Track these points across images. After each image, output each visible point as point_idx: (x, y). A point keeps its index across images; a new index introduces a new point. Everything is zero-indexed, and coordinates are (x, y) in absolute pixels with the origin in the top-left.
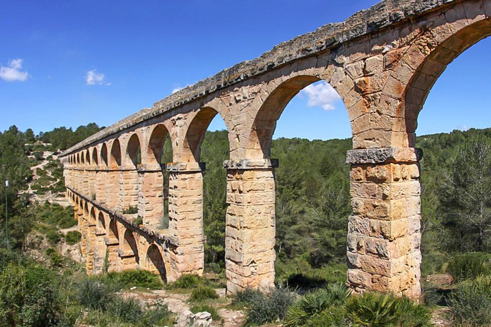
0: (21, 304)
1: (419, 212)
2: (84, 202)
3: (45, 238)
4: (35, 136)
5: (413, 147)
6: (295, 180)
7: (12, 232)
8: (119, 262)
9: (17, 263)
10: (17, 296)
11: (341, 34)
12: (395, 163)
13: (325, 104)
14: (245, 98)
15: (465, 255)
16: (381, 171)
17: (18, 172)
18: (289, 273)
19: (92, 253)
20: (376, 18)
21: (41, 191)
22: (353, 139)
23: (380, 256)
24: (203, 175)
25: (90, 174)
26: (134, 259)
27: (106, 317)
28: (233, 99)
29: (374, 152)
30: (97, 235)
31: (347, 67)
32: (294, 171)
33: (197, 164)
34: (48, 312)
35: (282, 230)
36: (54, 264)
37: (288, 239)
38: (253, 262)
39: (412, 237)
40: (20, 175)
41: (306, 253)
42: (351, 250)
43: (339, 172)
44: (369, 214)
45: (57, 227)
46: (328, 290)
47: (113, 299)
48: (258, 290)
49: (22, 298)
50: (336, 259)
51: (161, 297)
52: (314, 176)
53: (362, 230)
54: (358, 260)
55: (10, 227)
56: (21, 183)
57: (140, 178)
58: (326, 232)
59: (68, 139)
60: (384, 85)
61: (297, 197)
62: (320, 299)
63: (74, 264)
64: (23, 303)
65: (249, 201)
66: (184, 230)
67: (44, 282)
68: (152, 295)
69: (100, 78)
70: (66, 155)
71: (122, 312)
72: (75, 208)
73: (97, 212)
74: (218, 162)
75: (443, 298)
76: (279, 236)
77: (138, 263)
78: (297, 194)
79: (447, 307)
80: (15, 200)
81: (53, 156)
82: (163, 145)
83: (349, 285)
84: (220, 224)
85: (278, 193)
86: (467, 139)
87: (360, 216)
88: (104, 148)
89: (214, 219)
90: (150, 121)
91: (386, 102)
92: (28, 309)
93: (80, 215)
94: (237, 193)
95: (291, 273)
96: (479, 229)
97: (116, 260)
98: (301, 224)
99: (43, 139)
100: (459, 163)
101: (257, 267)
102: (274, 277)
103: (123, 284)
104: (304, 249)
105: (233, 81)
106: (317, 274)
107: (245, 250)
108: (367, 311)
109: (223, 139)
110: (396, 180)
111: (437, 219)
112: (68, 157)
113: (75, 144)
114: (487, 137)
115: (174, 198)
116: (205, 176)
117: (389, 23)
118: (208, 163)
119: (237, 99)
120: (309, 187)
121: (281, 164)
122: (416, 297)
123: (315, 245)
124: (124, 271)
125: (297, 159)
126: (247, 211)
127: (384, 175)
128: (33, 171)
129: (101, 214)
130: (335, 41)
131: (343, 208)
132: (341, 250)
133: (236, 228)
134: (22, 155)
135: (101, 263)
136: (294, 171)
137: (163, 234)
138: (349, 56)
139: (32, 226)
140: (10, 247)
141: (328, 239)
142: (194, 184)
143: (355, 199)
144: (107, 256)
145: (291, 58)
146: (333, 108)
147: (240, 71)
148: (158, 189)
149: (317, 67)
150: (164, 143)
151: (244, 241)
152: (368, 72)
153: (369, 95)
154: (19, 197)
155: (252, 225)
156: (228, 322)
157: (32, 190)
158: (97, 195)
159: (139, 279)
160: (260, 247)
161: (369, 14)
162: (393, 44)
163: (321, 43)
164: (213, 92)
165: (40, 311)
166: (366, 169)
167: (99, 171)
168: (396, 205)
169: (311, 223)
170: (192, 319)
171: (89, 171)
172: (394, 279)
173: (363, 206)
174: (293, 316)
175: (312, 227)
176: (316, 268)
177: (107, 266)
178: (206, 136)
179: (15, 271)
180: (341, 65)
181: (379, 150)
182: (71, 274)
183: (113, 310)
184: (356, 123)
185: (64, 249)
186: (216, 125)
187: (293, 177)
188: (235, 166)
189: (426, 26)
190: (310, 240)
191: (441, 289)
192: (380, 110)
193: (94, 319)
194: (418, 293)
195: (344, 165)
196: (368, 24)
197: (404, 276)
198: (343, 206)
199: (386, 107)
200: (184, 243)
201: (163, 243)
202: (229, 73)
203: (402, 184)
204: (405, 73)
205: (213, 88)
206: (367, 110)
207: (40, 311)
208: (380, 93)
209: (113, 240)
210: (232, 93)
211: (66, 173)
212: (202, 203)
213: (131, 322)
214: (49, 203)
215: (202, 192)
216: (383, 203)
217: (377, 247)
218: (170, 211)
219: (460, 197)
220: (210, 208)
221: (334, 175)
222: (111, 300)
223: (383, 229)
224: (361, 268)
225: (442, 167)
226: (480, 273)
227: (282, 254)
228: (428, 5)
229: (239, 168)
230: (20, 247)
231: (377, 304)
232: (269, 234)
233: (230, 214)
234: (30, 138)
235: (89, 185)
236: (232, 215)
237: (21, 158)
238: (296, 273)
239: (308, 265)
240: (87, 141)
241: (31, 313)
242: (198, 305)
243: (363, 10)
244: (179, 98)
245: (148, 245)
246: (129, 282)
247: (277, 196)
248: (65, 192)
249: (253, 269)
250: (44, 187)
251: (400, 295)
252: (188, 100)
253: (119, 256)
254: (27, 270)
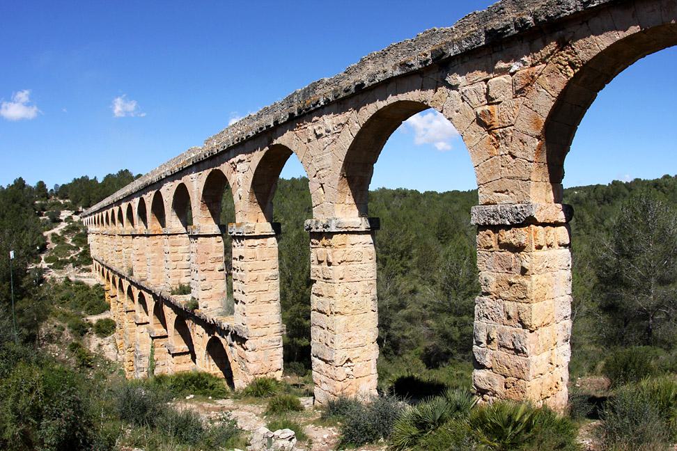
0: (39, 419)
1: (570, 292)
2: (117, 279)
3: (67, 329)
4: (49, 191)
5: (561, 203)
6: (403, 247)
7: (21, 320)
8: (169, 362)
9: (30, 362)
10: (33, 407)
11: (451, 44)
12: (537, 225)
13: (438, 141)
14: (328, 131)
15: (627, 350)
16: (518, 236)
17: (27, 239)
18: (396, 375)
19: (131, 349)
20: (496, 24)
21: (60, 265)
22: (479, 191)
23: (517, 351)
24: (278, 240)
25: (124, 240)
26: (189, 357)
27: (156, 436)
28: (311, 133)
29: (508, 209)
30: (138, 324)
31: (463, 91)
32: (400, 235)
33: (269, 225)
34: (77, 429)
35: (387, 316)
36: (81, 363)
37: (395, 329)
38: (348, 360)
39: (560, 326)
40: (30, 244)
41: (419, 348)
42: (479, 343)
43: (462, 236)
44: (502, 295)
45: (83, 313)
46: (447, 399)
47: (164, 412)
48: (356, 399)
49: (40, 410)
50: (459, 356)
51: (228, 409)
52: (428, 242)
53: (493, 316)
54: (488, 358)
55: (18, 314)
56: (31, 255)
57: (192, 245)
58: (446, 318)
59: (92, 192)
60: (516, 117)
61: (406, 271)
62: (437, 411)
63: (108, 364)
64: (42, 417)
65: (341, 277)
66: (255, 317)
67: (68, 389)
68: (215, 406)
69: (131, 107)
70: (91, 215)
71: (177, 429)
72: (106, 288)
73: (136, 292)
74: (297, 223)
75: (595, 408)
76: (383, 324)
77: (195, 362)
78: (406, 267)
79: (598, 421)
80: (23, 277)
81: (74, 217)
82: (221, 199)
83: (475, 392)
84: (304, 308)
85: (381, 266)
86: (631, 193)
87: (491, 296)
88: (142, 203)
89: (295, 301)
90: (201, 165)
91: (521, 141)
92: (49, 425)
93: (112, 297)
94: (325, 265)
95: (399, 375)
96: (648, 315)
97: (165, 359)
98: (412, 308)
99: (59, 195)
100: (621, 226)
101: (353, 368)
102: (377, 381)
103: (175, 392)
104: (417, 342)
105: (310, 108)
106: (433, 376)
107: (338, 344)
108: (496, 427)
109: (301, 190)
110: (539, 248)
111: (593, 301)
112: (93, 216)
113: (102, 199)
114: (658, 190)
115: (240, 272)
116: (280, 242)
117: (515, 32)
118: (284, 224)
119: (318, 132)
120: (422, 257)
121: (383, 226)
122: (560, 408)
123: (431, 337)
124: (176, 374)
125: (404, 219)
126: (339, 290)
127: (523, 242)
128: (46, 237)
129: (141, 295)
130: (444, 54)
131: (468, 286)
132: (465, 344)
133: (325, 314)
134: (32, 216)
135: (145, 363)
136: (400, 235)
137: (226, 323)
138: (465, 75)
139: (48, 312)
140: (18, 341)
141: (448, 329)
142: (266, 254)
143: (484, 274)
144: (152, 353)
145: (386, 76)
146: (449, 147)
147: (318, 94)
148: (217, 260)
149: (423, 89)
150: (222, 195)
151: (337, 332)
152: (493, 99)
153: (497, 131)
154: (29, 273)
155: (347, 310)
156: (317, 442)
157: (47, 262)
158: (134, 268)
159: (197, 384)
160: (358, 340)
161: (485, 18)
162: (523, 61)
163: (426, 55)
164: (285, 123)
165: (67, 428)
166: (498, 232)
167: (136, 235)
168: (539, 281)
169: (425, 307)
170: (270, 439)
171: (123, 236)
172: (533, 383)
173: (495, 284)
174: (401, 434)
175: (426, 312)
176: (433, 368)
177: (153, 367)
178: (279, 186)
179: (27, 373)
180: (455, 87)
181: (514, 206)
182: (104, 377)
183: (165, 427)
184: (482, 169)
185: (93, 343)
186: (291, 171)
187: (400, 243)
188: (320, 227)
189: (564, 38)
190: (424, 330)
191: (594, 397)
192: (512, 151)
193: (140, 440)
194: (563, 403)
195: (468, 228)
196: (485, 31)
197: (547, 380)
198: (468, 283)
199: (521, 147)
201: (227, 335)
202: (304, 97)
203: (546, 253)
204: (543, 102)
205: (283, 117)
206: (495, 152)
207: (67, 428)
208: (512, 128)
209: (160, 331)
210: (310, 124)
211: (91, 239)
212: (278, 279)
213: (190, 444)
214: (70, 281)
215: (277, 265)
216: (522, 279)
217: (513, 339)
218: (235, 291)
219: (624, 271)
220: (289, 286)
221: (455, 241)
222: (161, 413)
223: (521, 315)
224: (491, 368)
225: (600, 231)
226: (645, 375)
227: (387, 350)
228: (563, 9)
229: (326, 231)
230: (34, 340)
231: (510, 417)
232: (370, 321)
233: (316, 295)
234: (41, 194)
235: (124, 255)
236: (319, 295)
237: (31, 220)
238: (406, 375)
239: (422, 364)
240: (119, 195)
241: (54, 430)
242: (277, 420)
243: (477, 12)
244: (239, 132)
245: (207, 338)
246: (183, 388)
247: (379, 270)
248: (90, 266)
249: (348, 370)
251: (540, 404)
252: (251, 135)
253: (169, 353)
254: (44, 372)
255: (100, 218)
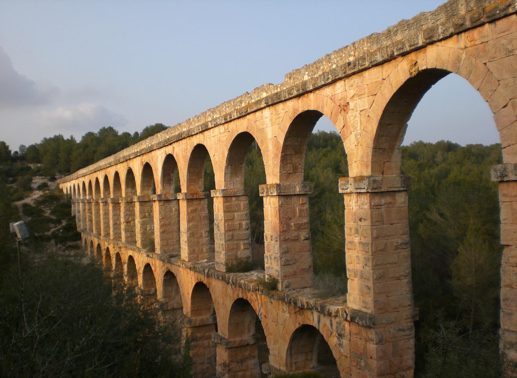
200: (384, 321)
248: (79, 242)
250: (41, 234)
255: (93, 184)
